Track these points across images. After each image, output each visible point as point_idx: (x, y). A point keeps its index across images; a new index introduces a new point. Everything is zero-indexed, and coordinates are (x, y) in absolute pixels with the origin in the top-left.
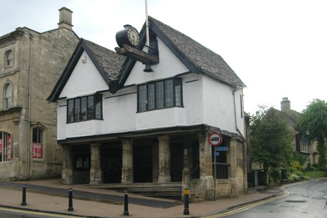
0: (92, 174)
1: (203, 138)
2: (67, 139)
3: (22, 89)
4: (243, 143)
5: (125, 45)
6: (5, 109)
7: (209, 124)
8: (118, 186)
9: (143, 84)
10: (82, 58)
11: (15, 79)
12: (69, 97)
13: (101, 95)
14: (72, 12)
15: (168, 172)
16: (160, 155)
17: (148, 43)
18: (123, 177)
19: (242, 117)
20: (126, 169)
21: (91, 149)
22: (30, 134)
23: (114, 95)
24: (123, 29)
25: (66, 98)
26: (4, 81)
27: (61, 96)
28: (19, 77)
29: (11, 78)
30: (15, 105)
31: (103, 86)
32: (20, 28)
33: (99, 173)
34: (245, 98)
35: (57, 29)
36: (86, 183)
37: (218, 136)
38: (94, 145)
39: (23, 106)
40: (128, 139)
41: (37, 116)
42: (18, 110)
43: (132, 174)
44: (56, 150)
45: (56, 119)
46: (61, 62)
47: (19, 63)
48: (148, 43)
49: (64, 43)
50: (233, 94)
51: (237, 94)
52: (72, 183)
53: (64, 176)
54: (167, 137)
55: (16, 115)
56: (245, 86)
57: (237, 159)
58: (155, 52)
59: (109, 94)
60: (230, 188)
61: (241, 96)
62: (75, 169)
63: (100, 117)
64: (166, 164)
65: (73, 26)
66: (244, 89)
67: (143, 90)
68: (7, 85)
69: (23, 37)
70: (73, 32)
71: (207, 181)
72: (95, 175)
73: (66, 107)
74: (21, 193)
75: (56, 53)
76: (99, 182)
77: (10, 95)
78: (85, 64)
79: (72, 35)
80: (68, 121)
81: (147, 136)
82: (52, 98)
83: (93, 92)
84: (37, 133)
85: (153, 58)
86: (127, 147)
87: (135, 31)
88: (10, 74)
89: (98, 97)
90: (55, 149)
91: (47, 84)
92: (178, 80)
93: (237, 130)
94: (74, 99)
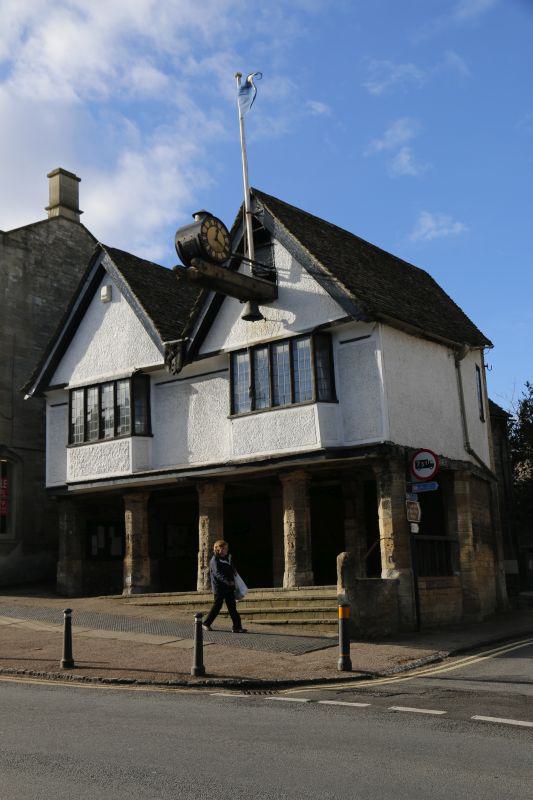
1: (385, 477)
7: (401, 441)
9: (242, 351)
14: (79, 180)
17: (250, 254)
19: (483, 421)
34: (490, 377)
35: (44, 222)
37: (416, 471)
38: (130, 497)
46: (55, 301)
48: (250, 254)
51: (469, 363)
53: (61, 576)
54: (300, 476)
56: (490, 345)
61: (478, 369)
65: (81, 212)
66: (489, 355)
70: (82, 226)
73: (67, 407)
83: (130, 370)
86: (209, 498)
87: (220, 226)
93: (471, 452)
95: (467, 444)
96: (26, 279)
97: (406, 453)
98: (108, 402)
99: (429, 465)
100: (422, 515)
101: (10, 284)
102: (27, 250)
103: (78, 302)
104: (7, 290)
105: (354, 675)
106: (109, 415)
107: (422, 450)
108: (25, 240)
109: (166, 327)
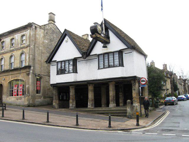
2: (57, 83)
3: (31, 56)
5: (96, 33)
6: (21, 67)
7: (138, 76)
8: (87, 110)
11: (27, 50)
12: (58, 61)
13: (76, 60)
14: (55, 15)
15: (115, 102)
16: (110, 92)
18: (89, 104)
20: (91, 100)
22: (35, 81)
23: (85, 60)
24: (93, 25)
25: (56, 61)
27: (53, 60)
28: (30, 49)
29: (24, 50)
30: (27, 64)
31: (78, 55)
32: (30, 23)
33: (74, 103)
37: (141, 82)
39: (32, 65)
41: (38, 71)
42: (29, 67)
43: (94, 103)
47: (30, 42)
49: (51, 31)
50: (145, 60)
53: (54, 104)
54: (114, 83)
55: (28, 70)
58: (108, 37)
59: (82, 59)
64: (113, 97)
65: (55, 22)
69: (32, 28)
72: (72, 104)
73: (56, 66)
74: (47, 114)
76: (74, 107)
77: (24, 59)
79: (55, 27)
80: (58, 74)
82: (48, 61)
83: (73, 57)
84: (39, 79)
85: (107, 40)
86: (91, 88)
88: (24, 48)
89: (75, 60)
92: (121, 52)
96: (44, 36)
97: (139, 78)
98: (106, 62)
99: (144, 81)
102: (44, 30)
105: (140, 127)
107: (143, 78)
108: (44, 28)
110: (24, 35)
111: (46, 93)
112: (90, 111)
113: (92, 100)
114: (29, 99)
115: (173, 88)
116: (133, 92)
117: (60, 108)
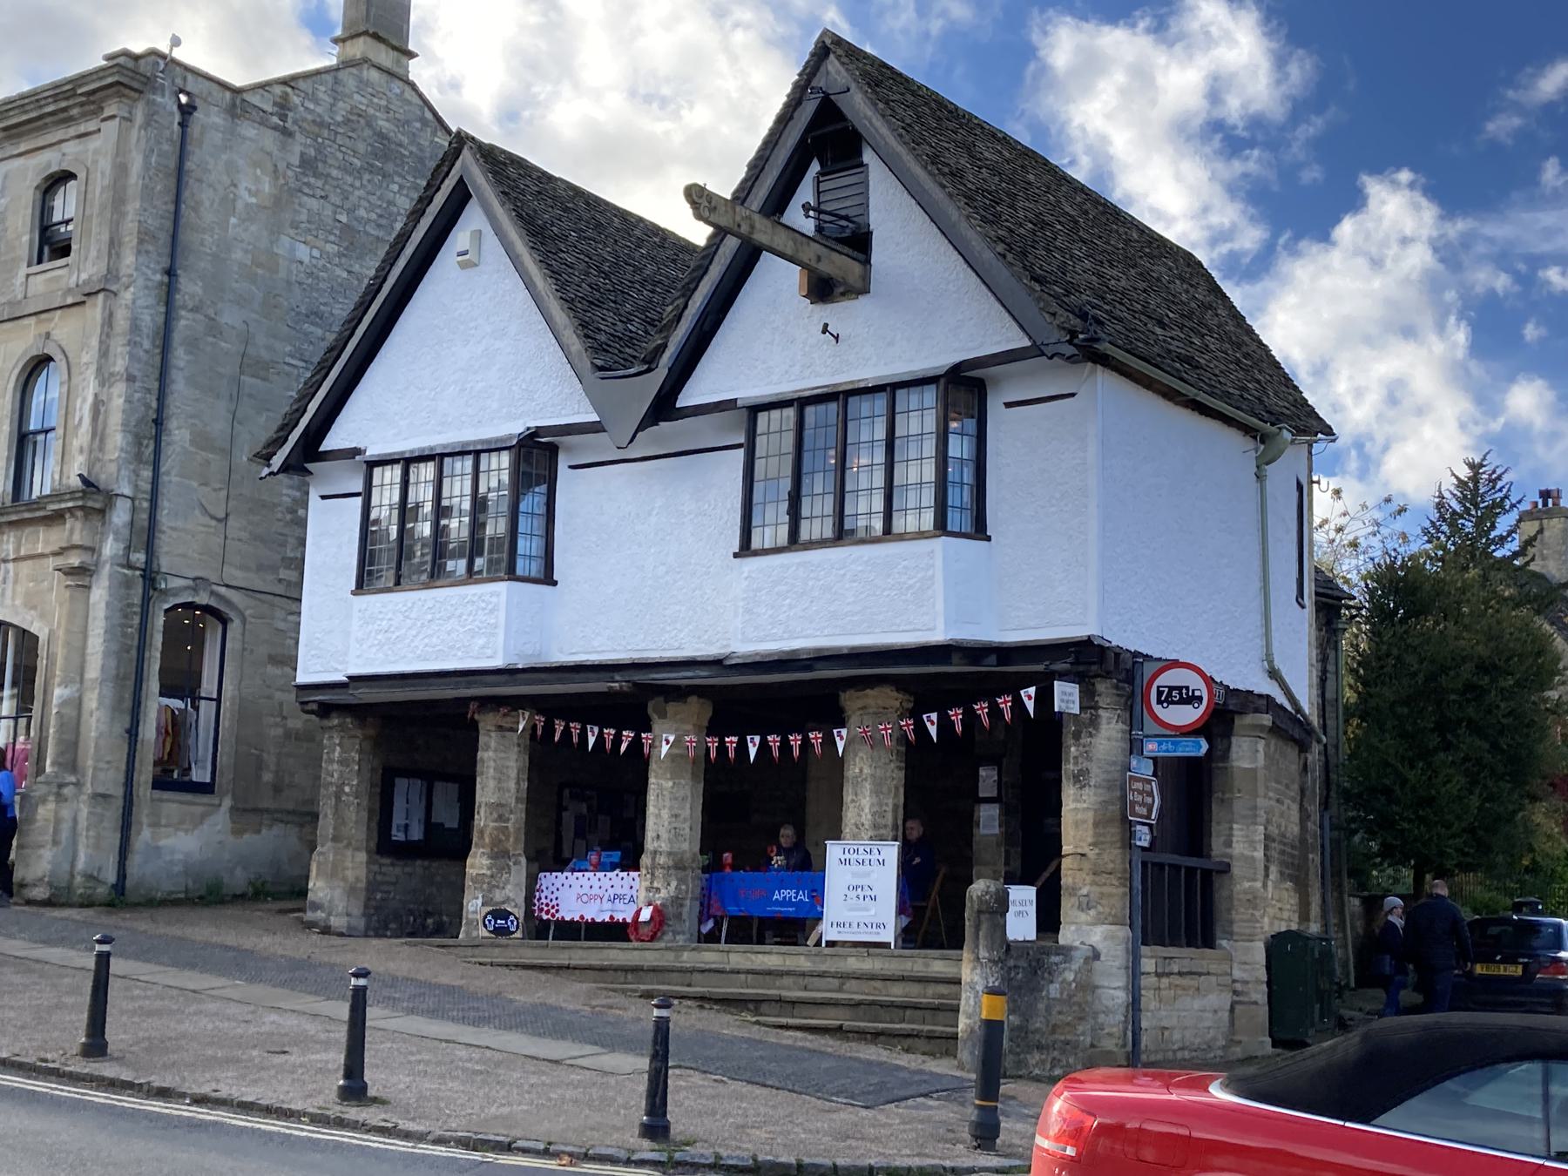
0: (478, 879)
4: (1303, 748)
10: (460, 238)
12: (373, 451)
13: (553, 450)
20: (662, 860)
21: (482, 739)
25: (355, 452)
26: (21, 343)
27: (331, 442)
28: (109, 321)
32: (126, 54)
36: (439, 931)
37: (1157, 709)
40: (677, 694)
44: (288, 735)
45: (299, 564)
46: (340, 255)
50: (1260, 477)
52: (361, 924)
53: (318, 887)
57: (1267, 837)
60: (1226, 999)
61: (1300, 487)
62: (385, 846)
63: (535, 569)
65: (411, 55)
67: (776, 429)
68: (40, 363)
70: (413, 86)
71: (1096, 955)
75: (314, 204)
78: (471, 272)
81: (782, 684)
83: (514, 428)
90: (280, 731)
91: (261, 368)
93: (1274, 674)
94: (801, 403)
95: (1269, 658)
98: (422, 493)
99: (1191, 699)
100: (1161, 809)
101: (240, 205)
103: (401, 263)
104: (233, 220)
106: (458, 527)
107: (1175, 664)
108: (283, 106)
109: (603, 338)
110: (64, 177)
111: (267, 777)
112: (636, 970)
113: (679, 866)
114: (66, 827)
115: (237, 701)
116: (1069, 793)
117: (379, 934)
